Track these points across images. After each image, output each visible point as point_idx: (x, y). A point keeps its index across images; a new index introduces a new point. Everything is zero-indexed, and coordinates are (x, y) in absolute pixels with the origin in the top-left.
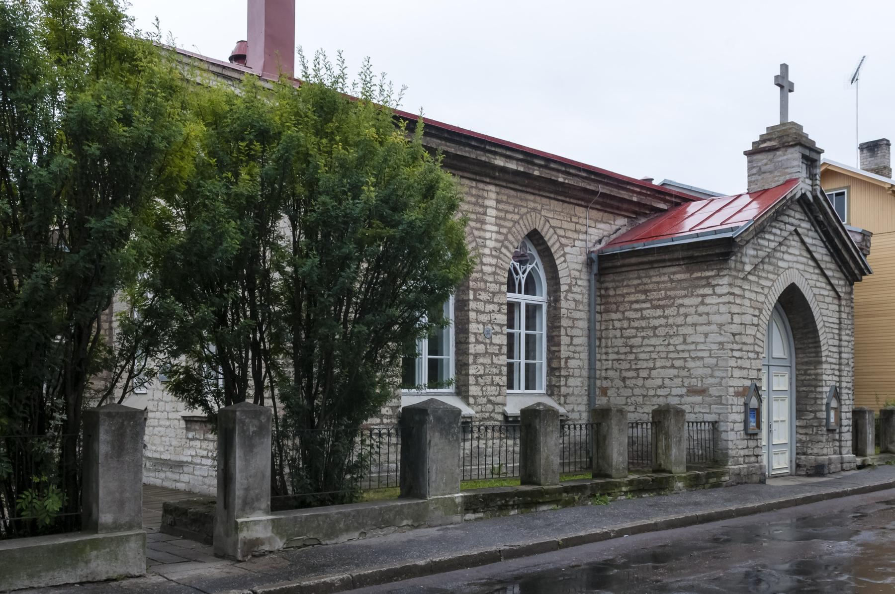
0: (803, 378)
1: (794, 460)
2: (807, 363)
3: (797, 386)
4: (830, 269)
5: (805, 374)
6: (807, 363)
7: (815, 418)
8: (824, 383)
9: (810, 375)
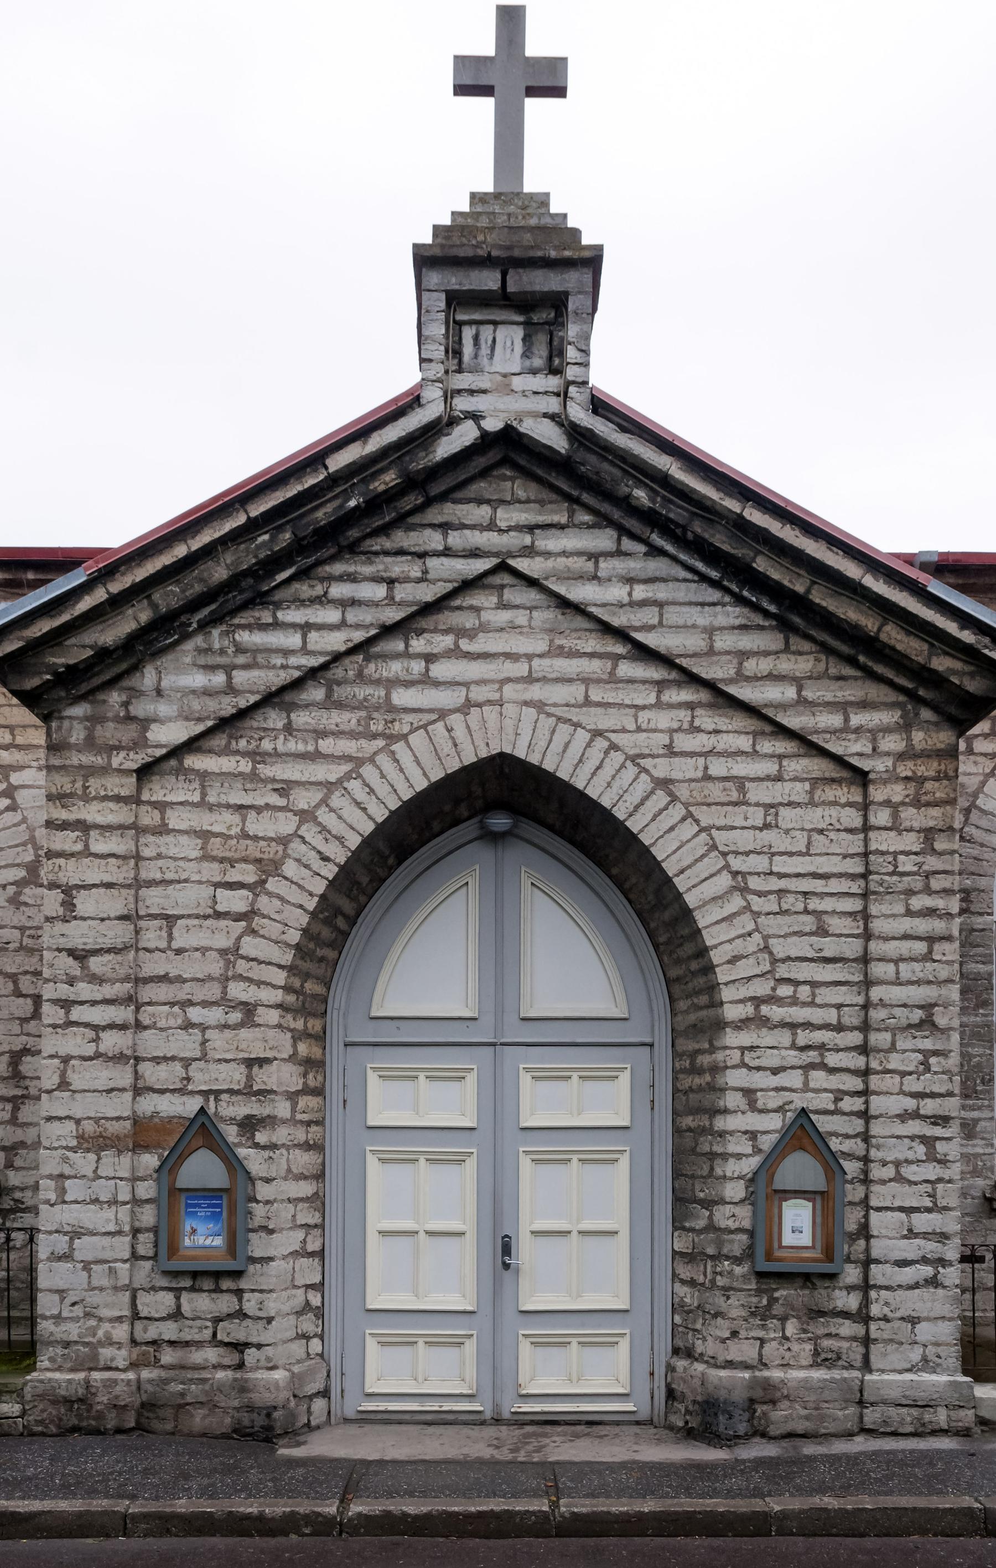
1: (660, 1371)
7: (711, 1227)
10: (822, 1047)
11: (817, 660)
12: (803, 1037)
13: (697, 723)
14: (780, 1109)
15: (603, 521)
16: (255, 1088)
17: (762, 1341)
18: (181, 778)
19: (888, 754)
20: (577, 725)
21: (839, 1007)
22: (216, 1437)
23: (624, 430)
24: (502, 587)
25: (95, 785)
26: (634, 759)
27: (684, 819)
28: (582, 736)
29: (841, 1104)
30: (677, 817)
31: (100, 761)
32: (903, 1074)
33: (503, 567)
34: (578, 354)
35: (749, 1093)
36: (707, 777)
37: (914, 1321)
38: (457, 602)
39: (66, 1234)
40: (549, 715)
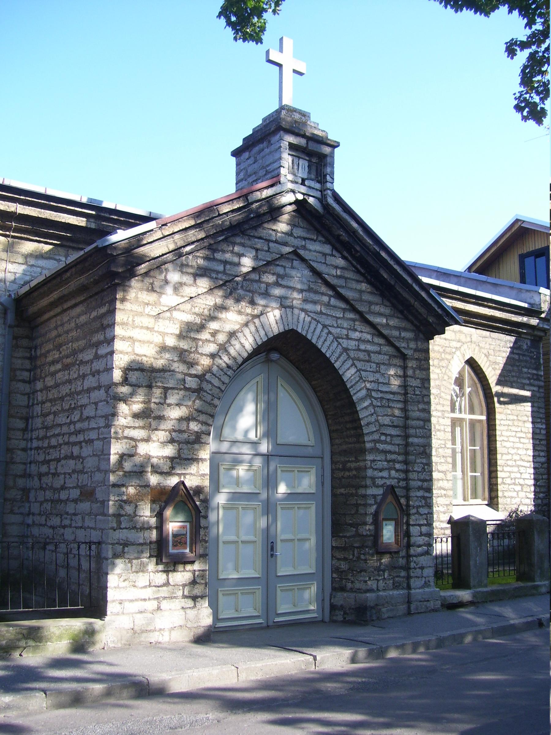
0: (341, 474)
2: (345, 453)
3: (333, 487)
4: (381, 314)
5: (344, 469)
6: (345, 453)
7: (357, 535)
8: (369, 482)
9: (350, 470)
10: (394, 461)
11: (391, 309)
12: (389, 457)
13: (355, 327)
14: (382, 486)
15: (328, 241)
16: (200, 473)
17: (378, 580)
18: (172, 322)
19: (411, 349)
20: (318, 322)
21: (398, 445)
22: (165, 649)
23: (345, 212)
24: (293, 260)
25: (138, 320)
26: (336, 338)
27: (352, 366)
28: (320, 327)
29: (400, 484)
30: (350, 365)
31: (140, 309)
32: (419, 472)
33: (295, 253)
34: (331, 179)
35: (373, 479)
36: (359, 350)
37: (422, 568)
38: (278, 263)
39: (121, 545)
40: (309, 316)
